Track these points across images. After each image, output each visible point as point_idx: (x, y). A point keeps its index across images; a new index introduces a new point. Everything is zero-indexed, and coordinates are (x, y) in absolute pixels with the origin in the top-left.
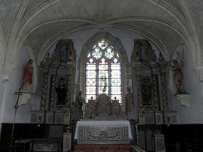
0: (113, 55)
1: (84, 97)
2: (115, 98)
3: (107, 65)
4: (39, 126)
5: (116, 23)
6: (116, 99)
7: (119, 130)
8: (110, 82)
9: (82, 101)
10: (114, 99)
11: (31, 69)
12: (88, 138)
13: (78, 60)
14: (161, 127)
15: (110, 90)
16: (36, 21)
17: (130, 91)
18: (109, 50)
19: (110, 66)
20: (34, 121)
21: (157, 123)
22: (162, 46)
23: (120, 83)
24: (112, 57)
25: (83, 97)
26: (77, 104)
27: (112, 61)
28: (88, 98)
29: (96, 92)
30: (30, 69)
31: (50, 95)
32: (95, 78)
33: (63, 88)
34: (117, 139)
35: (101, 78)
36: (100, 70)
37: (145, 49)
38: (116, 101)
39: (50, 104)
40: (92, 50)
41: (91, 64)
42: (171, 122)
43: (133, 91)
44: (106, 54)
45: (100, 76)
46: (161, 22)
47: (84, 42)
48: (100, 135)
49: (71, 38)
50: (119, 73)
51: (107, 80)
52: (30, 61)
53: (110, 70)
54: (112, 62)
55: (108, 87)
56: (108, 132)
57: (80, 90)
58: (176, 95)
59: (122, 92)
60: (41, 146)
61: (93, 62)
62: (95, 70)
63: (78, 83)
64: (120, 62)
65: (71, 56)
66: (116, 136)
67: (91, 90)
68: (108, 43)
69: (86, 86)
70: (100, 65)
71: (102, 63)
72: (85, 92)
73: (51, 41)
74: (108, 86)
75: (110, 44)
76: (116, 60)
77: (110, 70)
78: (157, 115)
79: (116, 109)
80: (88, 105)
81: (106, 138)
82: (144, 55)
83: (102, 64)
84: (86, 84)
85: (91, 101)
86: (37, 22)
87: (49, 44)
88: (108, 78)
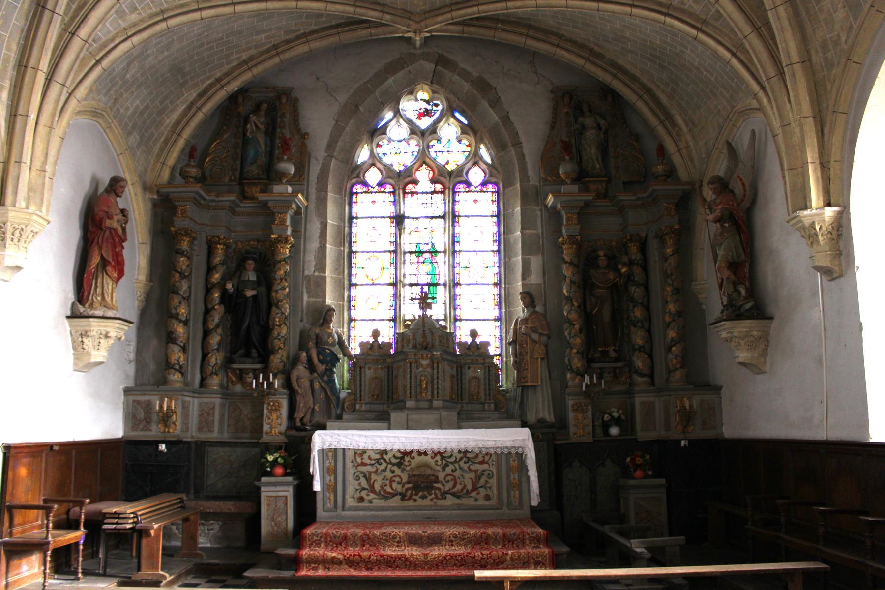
0: (466, 154)
1: (345, 330)
2: (474, 334)
3: (441, 196)
4: (163, 447)
5: (478, 19)
6: (478, 340)
7: (485, 466)
8: (454, 267)
9: (333, 349)
10: (469, 340)
11: (120, 217)
12: (361, 499)
13: (319, 174)
14: (193, 445)
16: (132, 13)
17: (535, 307)
18: (449, 130)
19: (454, 201)
20: (142, 430)
21: (642, 435)
22: (669, 117)
23: (496, 270)
24: (461, 159)
25: (337, 333)
26: (315, 360)
27: (459, 179)
28: (358, 337)
29: (395, 309)
30: (116, 218)
32: (390, 251)
33: (254, 296)
34: (476, 500)
36: (408, 218)
37: (599, 127)
38: (476, 351)
40: (376, 132)
41: (371, 189)
42: (698, 432)
43: (545, 305)
44: (436, 147)
45: (409, 242)
46: (662, 18)
47: (343, 98)
48: (407, 486)
50: (490, 227)
52: (116, 185)
53: (454, 216)
54: (461, 183)
56: (441, 476)
58: (719, 324)
59: (503, 310)
60: (174, 527)
61: (380, 184)
62: (390, 217)
63: (316, 274)
64: (495, 184)
65: (289, 160)
66: (475, 488)
68: (444, 100)
69: (351, 285)
70: (412, 193)
71: (419, 188)
72: (349, 309)
73: (200, 96)
75: (455, 105)
76: (476, 175)
77: (452, 217)
78: (643, 403)
79: (476, 378)
80: (357, 365)
81: (431, 500)
82: (592, 152)
83: (417, 190)
84: (350, 275)
86: (134, 17)
87: (194, 109)
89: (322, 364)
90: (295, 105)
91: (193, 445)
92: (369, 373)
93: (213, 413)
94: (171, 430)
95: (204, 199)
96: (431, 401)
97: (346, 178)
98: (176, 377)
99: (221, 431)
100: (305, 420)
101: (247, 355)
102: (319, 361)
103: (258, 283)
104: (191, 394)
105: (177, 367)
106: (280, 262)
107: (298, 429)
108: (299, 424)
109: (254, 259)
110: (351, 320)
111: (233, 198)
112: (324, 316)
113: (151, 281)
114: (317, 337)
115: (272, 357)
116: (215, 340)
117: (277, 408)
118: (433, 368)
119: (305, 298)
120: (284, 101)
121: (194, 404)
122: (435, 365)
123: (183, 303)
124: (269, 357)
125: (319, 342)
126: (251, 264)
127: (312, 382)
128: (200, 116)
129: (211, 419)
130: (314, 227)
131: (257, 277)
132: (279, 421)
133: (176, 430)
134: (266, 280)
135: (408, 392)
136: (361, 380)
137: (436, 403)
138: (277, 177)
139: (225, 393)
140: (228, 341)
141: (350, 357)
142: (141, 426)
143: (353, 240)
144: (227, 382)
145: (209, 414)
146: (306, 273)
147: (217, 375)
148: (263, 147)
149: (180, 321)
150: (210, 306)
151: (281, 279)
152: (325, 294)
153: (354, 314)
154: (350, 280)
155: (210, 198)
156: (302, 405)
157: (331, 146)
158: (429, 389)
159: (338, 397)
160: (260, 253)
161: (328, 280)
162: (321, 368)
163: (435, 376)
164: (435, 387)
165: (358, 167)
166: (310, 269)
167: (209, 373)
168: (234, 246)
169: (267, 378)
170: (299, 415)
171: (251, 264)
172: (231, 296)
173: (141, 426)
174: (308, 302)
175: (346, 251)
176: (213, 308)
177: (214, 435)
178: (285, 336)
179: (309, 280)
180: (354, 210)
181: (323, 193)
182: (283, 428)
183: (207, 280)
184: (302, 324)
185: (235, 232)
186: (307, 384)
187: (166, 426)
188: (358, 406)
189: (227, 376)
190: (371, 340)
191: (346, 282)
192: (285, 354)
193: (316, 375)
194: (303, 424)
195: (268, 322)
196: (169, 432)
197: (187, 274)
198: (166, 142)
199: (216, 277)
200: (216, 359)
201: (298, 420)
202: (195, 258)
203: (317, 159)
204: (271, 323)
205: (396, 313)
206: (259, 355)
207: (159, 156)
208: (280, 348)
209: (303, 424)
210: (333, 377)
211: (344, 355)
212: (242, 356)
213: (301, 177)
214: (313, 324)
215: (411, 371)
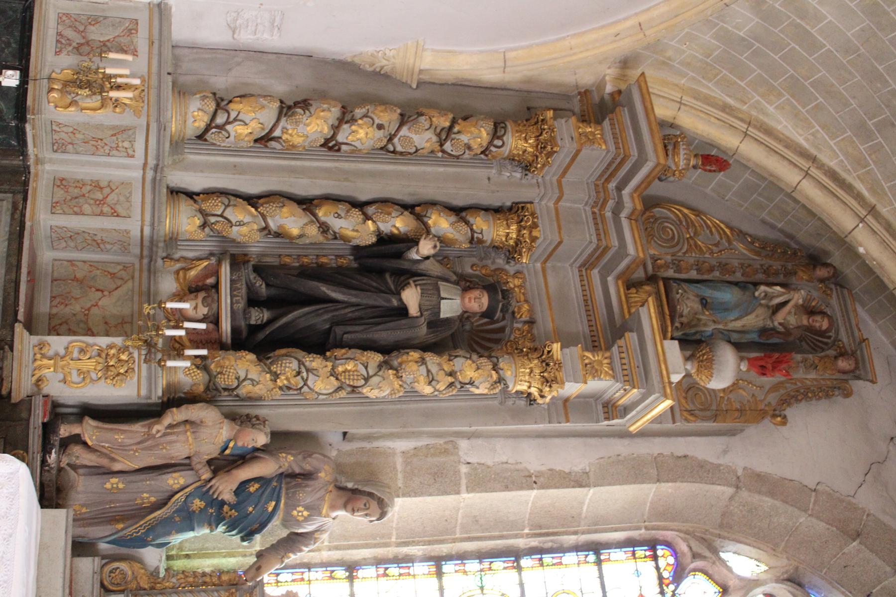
1: (326, 555)
9: (276, 522)
14: (17, 162)
20: (59, 34)
33: (402, 311)
39: (221, 193)
47: (868, 500)
49: (768, 381)
57: (399, 502)
63: (464, 469)
69: (438, 561)
72: (378, 562)
73: (833, 175)
84: (462, 557)
87: (803, 163)
89: (237, 493)
90: (836, 389)
91: (17, 162)
93: (102, 214)
94: (55, 95)
95: (619, 188)
97: (687, 526)
98: (196, 114)
99: (62, 237)
100: (77, 450)
101: (253, 301)
102: (244, 484)
103: (436, 323)
104: (152, 162)
105: (220, 119)
106: (495, 368)
107: (48, 429)
108: (65, 431)
109: (488, 314)
110: (352, 568)
111: (631, 249)
113: (420, 84)
114: (307, 476)
115: (252, 357)
116: (291, 221)
117: (110, 370)
119: (401, 445)
120: (842, 364)
121: (125, 170)
123: (380, 134)
124: (251, 350)
125: (297, 478)
126: (479, 302)
127: (185, 465)
128: (789, 176)
129: (87, 208)
130: (573, 456)
131: (447, 321)
132: (75, 377)
133: (50, 113)
134: (444, 339)
138: (694, 343)
139: (157, 249)
140: (287, 260)
141: (257, 568)
142: (69, 33)
143: (547, 559)
144: (185, 259)
145: (101, 202)
146: (463, 444)
147: (203, 226)
148: (738, 325)
149: (336, 128)
150: (371, 210)
151: (451, 374)
152: (416, 495)
153: (367, 572)
154: (449, 558)
155: (626, 199)
156: (120, 437)
157: (761, 482)
159: (142, 542)
160: (502, 330)
161: (449, 500)
162: (225, 488)
165: (715, 551)
167: (204, 206)
168: (511, 268)
169: (196, 339)
170: (90, 430)
171: (479, 302)
172: (399, 255)
173: (69, 33)
174: (391, 454)
175: (521, 543)
176: (367, 218)
177: (43, 217)
178: (310, 391)
179: (446, 452)
180: (618, 554)
181: (654, 472)
182: (55, 389)
183: (433, 204)
184: (334, 438)
185: (544, 270)
186: (179, 449)
187: (66, 83)
189: (199, 259)
192: (258, 390)
193: (206, 475)
194: (65, 444)
195: (341, 345)
196: (51, 90)
197: (448, 146)
198: (725, 108)
199: (441, 223)
200: (244, 226)
201: (76, 430)
202: (481, 173)
203: (725, 452)
204: (339, 352)
206: (254, 329)
207: (697, 96)
208: (276, 376)
209: (65, 444)
210: (201, 524)
211: (260, 555)
212: (250, 287)
213: (691, 412)
214: (340, 468)
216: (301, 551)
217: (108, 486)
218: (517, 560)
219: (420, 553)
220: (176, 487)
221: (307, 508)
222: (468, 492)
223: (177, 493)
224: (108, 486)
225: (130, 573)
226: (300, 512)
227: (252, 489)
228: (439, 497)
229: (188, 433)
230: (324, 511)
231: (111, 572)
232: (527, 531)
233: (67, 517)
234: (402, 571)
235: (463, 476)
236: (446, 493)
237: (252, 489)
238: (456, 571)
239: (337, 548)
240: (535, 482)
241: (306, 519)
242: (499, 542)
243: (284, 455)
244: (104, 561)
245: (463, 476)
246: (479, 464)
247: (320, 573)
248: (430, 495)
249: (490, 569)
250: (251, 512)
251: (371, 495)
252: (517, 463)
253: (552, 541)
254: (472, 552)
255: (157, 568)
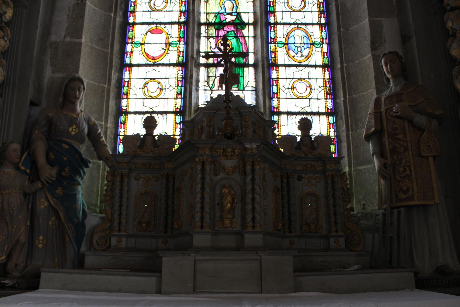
1: (110, 125)
8: (268, 43)
10: (297, 133)
15: (266, 87)
26: (41, 159)
31: (99, 269)
35: (212, 19)
51: (248, 32)
55: (251, 69)
63: (68, 39)
67: (153, 86)
74: (255, 66)
85: (149, 145)
88: (251, 21)
92: (136, 186)
96: (240, 234)
112: (68, 90)
114: (50, 123)
118: (244, 173)
122: (249, 167)
125: (52, 131)
127: (29, 197)
135: (198, 218)
136: (121, 197)
137: (251, 239)
146: (53, 38)
152: (78, 67)
158: (238, 211)
161: (84, 50)
162: (49, 172)
163: (249, 188)
164: (249, 207)
166: (59, 34)
175: (119, 20)
188: (114, 241)
190: (143, 132)
191: (116, 61)
205: (184, 102)
215: (203, 179)
216: (100, 134)
217: (40, 246)
218: (129, 24)
219: (117, 74)
220: (46, 204)
221: (71, 125)
222: (81, 38)
223: (50, 204)
224: (40, 246)
225: (100, 234)
226: (73, 131)
227: (53, 157)
228: (82, 55)
229: (4, 193)
230: (75, 116)
231: (98, 245)
232: (112, 15)
233: (47, 272)
234: (126, 85)
235: (72, 40)
236: (79, 52)
237: (53, 157)
238: (130, 57)
239: (107, 118)
240: (82, 1)
241: (78, 126)
242: (116, 30)
243: (34, 136)
244: (92, 249)
245: (72, 40)
246: (66, 31)
247: (121, 130)
248: (79, 59)
249: (132, 39)
250: (68, 158)
251: (67, 86)
252: (69, 10)
253: (121, 4)
254: (120, 46)
255: (101, 218)
